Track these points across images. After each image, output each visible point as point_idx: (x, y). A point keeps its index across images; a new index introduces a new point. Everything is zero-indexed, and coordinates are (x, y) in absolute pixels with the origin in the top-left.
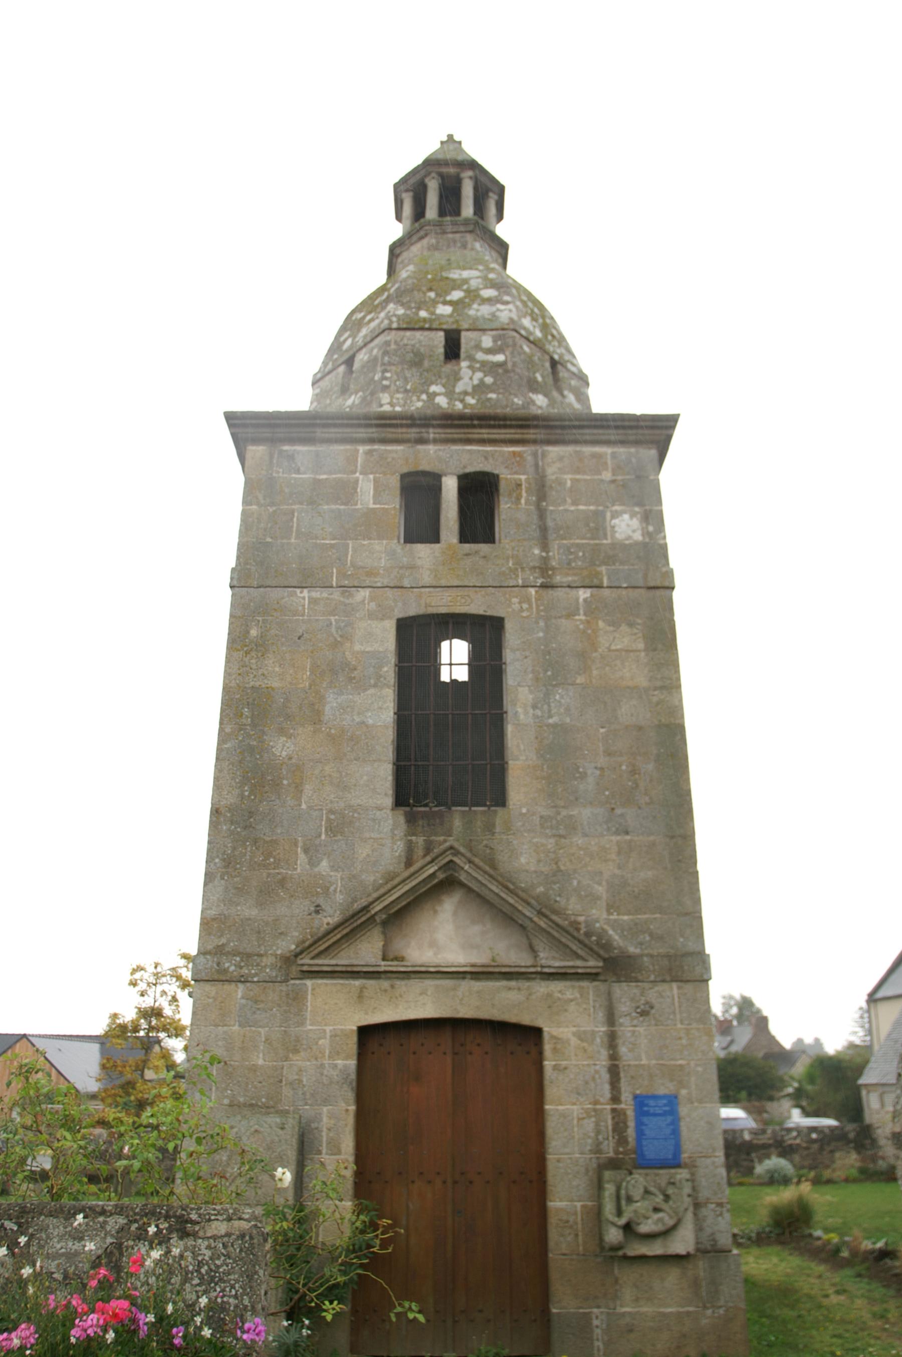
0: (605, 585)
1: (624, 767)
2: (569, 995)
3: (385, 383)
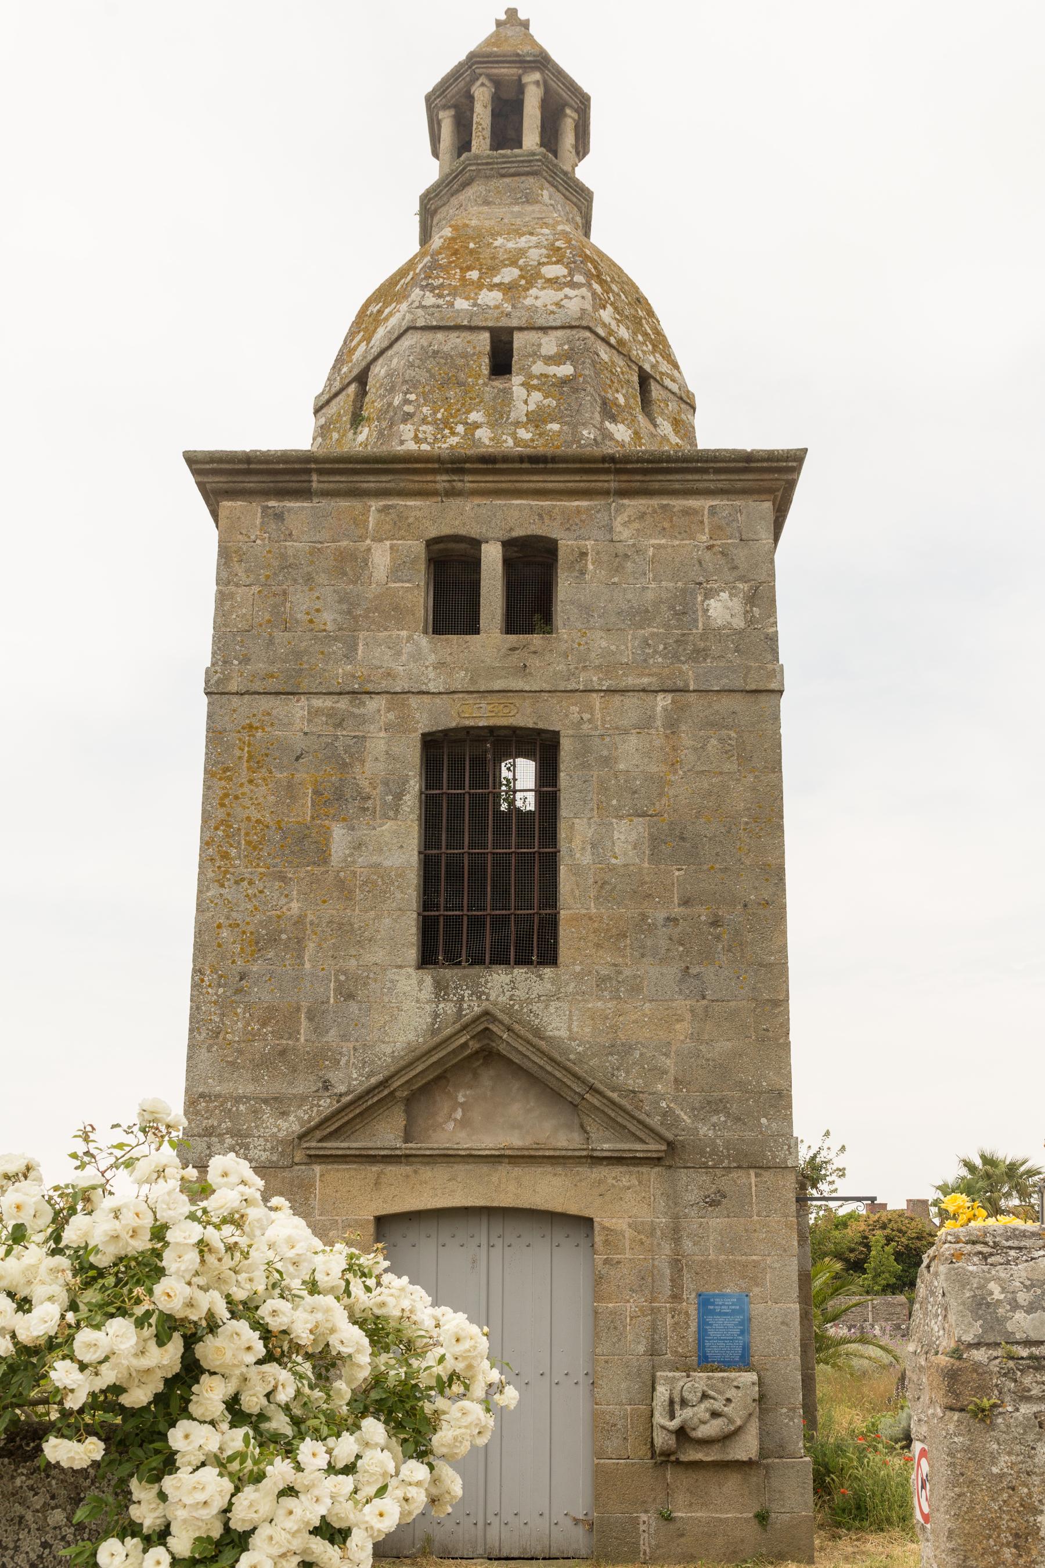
1: (703, 918)
3: (407, 408)
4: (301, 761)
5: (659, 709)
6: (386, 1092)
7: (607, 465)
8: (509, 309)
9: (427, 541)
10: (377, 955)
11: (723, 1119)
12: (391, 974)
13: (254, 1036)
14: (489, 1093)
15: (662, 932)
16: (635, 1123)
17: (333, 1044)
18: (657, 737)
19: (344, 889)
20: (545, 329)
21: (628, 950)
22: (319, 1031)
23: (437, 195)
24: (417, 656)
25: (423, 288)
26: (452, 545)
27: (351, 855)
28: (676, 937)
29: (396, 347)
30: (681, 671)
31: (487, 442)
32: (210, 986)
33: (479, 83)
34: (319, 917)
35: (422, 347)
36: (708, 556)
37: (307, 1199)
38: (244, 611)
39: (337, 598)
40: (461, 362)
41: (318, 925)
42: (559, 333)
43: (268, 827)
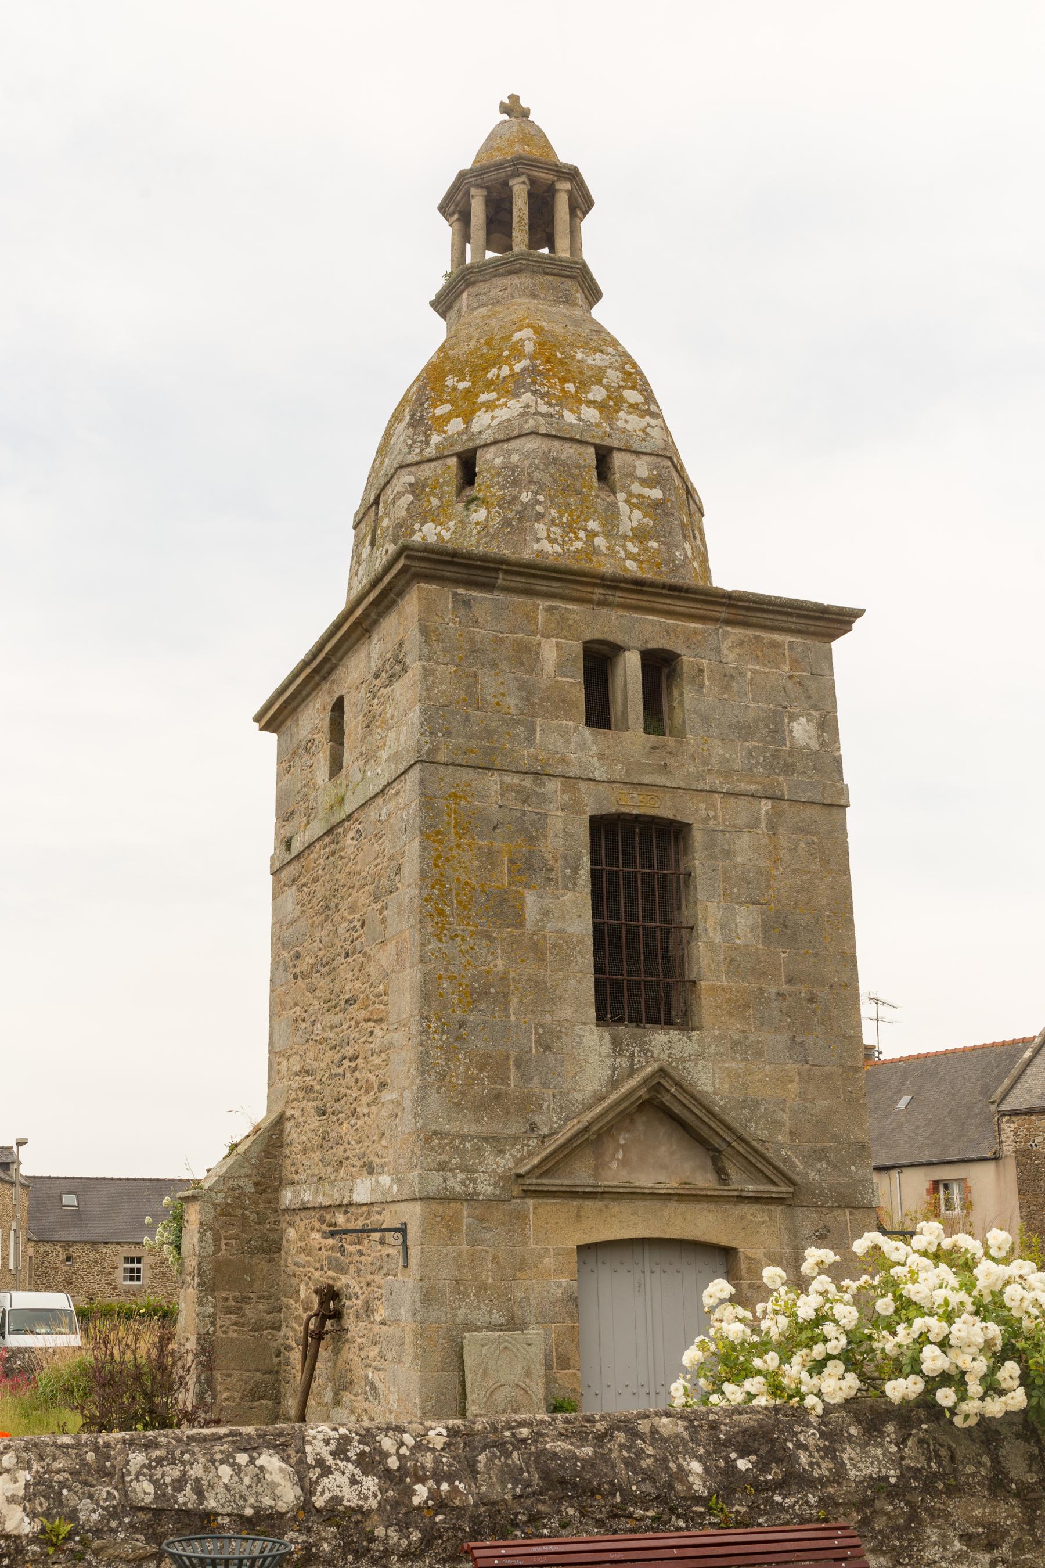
1: (803, 995)
3: (539, 509)
5: (763, 812)
10: (566, 1012)
12: (578, 1029)
13: (474, 1080)
14: (642, 1137)
15: (775, 1004)
19: (537, 951)
22: (525, 1078)
25: (535, 393)
26: (596, 646)
27: (541, 920)
28: (784, 1010)
36: (789, 685)
37: (523, 1230)
38: (444, 687)
40: (576, 471)
42: (649, 459)
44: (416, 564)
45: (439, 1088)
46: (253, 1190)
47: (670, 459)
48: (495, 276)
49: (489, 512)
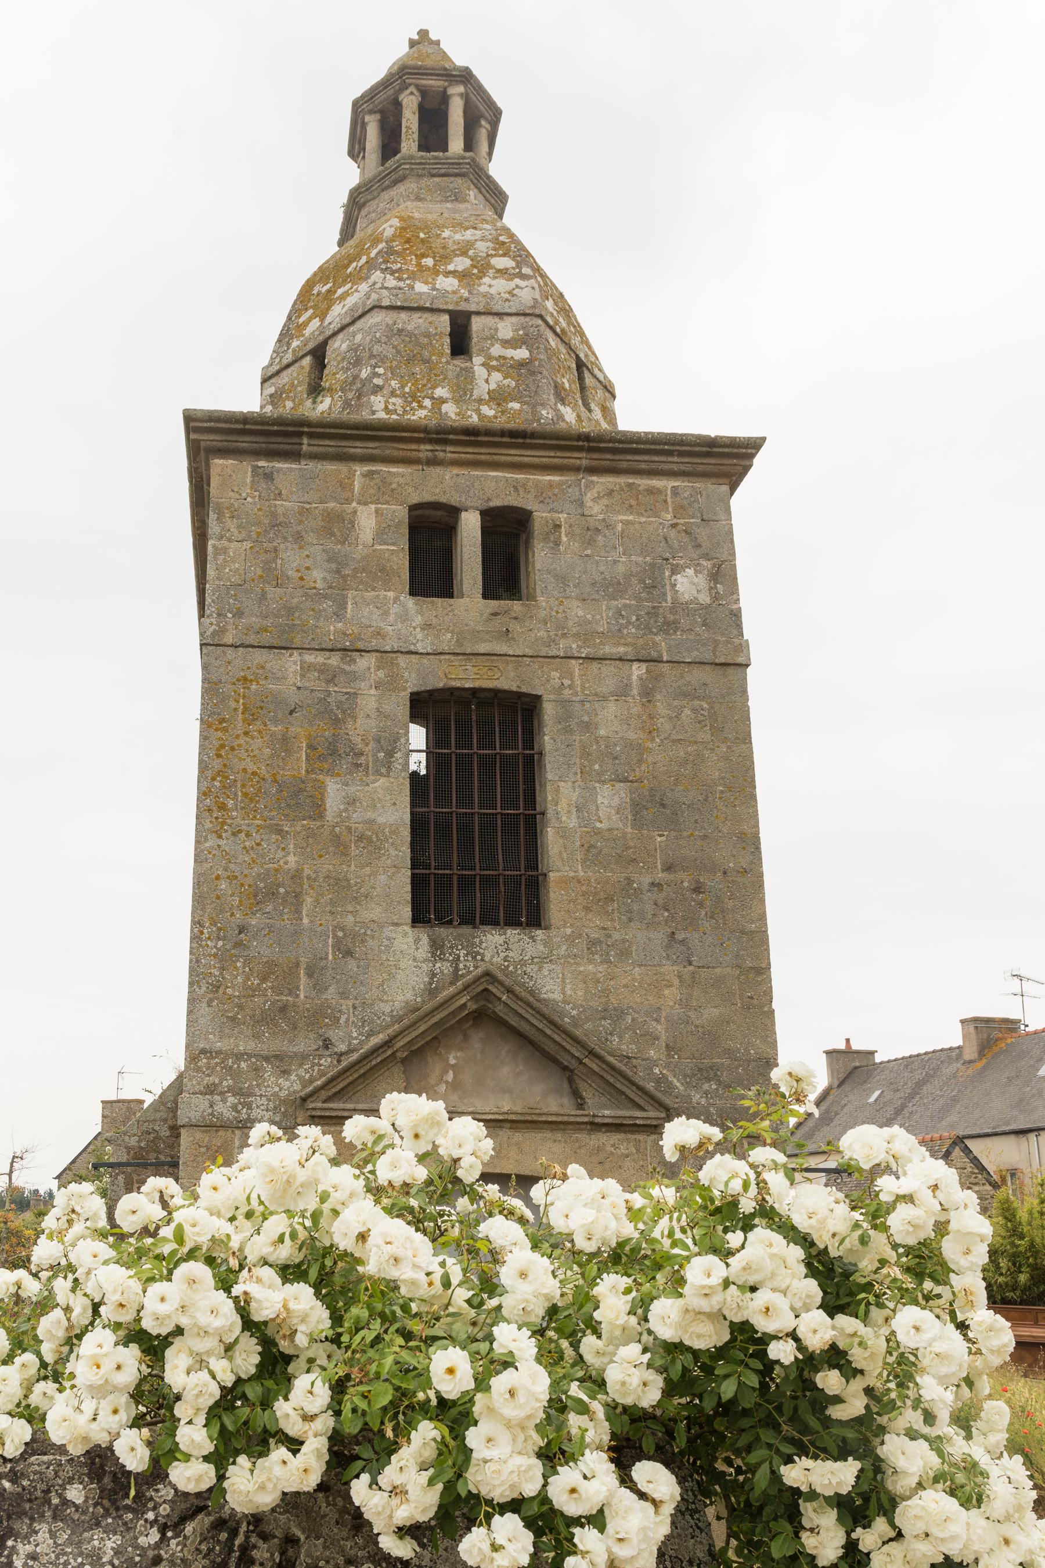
0: (665, 659)
1: (686, 884)
2: (623, 1149)
3: (377, 381)
4: (295, 715)
5: (635, 678)
6: (389, 1052)
7: (581, 443)
8: (466, 295)
9: (410, 507)
10: (374, 912)
11: (714, 1087)
12: (388, 931)
13: (254, 991)
14: (479, 1056)
16: (634, 1089)
17: (333, 1001)
18: (634, 704)
19: (339, 845)
20: (500, 315)
21: (616, 914)
22: (319, 988)
23: (367, 190)
24: (404, 617)
25: (383, 271)
26: (427, 512)
27: (346, 810)
28: (660, 902)
29: (359, 324)
30: (654, 642)
31: (453, 416)
32: (209, 938)
33: (408, 91)
34: (315, 872)
35: (387, 325)
36: (673, 534)
38: (237, 565)
39: (325, 557)
41: (315, 880)
42: (514, 319)
43: (264, 779)
44: (206, 437)
45: (211, 1000)
46: (168, 1133)
47: (541, 317)
48: (383, 190)
49: (333, 399)
